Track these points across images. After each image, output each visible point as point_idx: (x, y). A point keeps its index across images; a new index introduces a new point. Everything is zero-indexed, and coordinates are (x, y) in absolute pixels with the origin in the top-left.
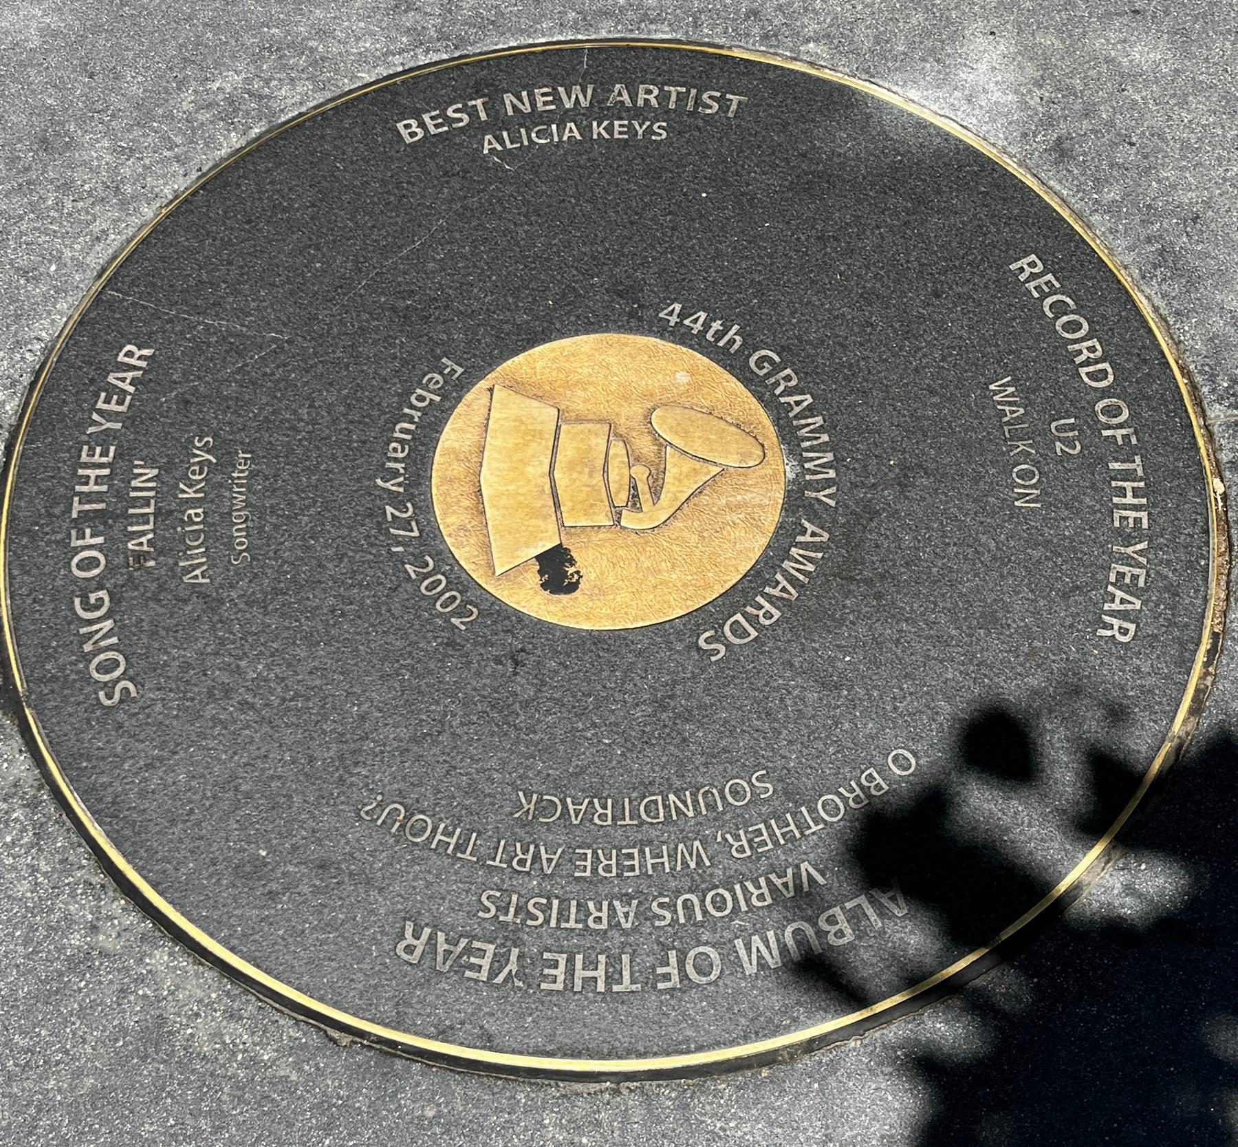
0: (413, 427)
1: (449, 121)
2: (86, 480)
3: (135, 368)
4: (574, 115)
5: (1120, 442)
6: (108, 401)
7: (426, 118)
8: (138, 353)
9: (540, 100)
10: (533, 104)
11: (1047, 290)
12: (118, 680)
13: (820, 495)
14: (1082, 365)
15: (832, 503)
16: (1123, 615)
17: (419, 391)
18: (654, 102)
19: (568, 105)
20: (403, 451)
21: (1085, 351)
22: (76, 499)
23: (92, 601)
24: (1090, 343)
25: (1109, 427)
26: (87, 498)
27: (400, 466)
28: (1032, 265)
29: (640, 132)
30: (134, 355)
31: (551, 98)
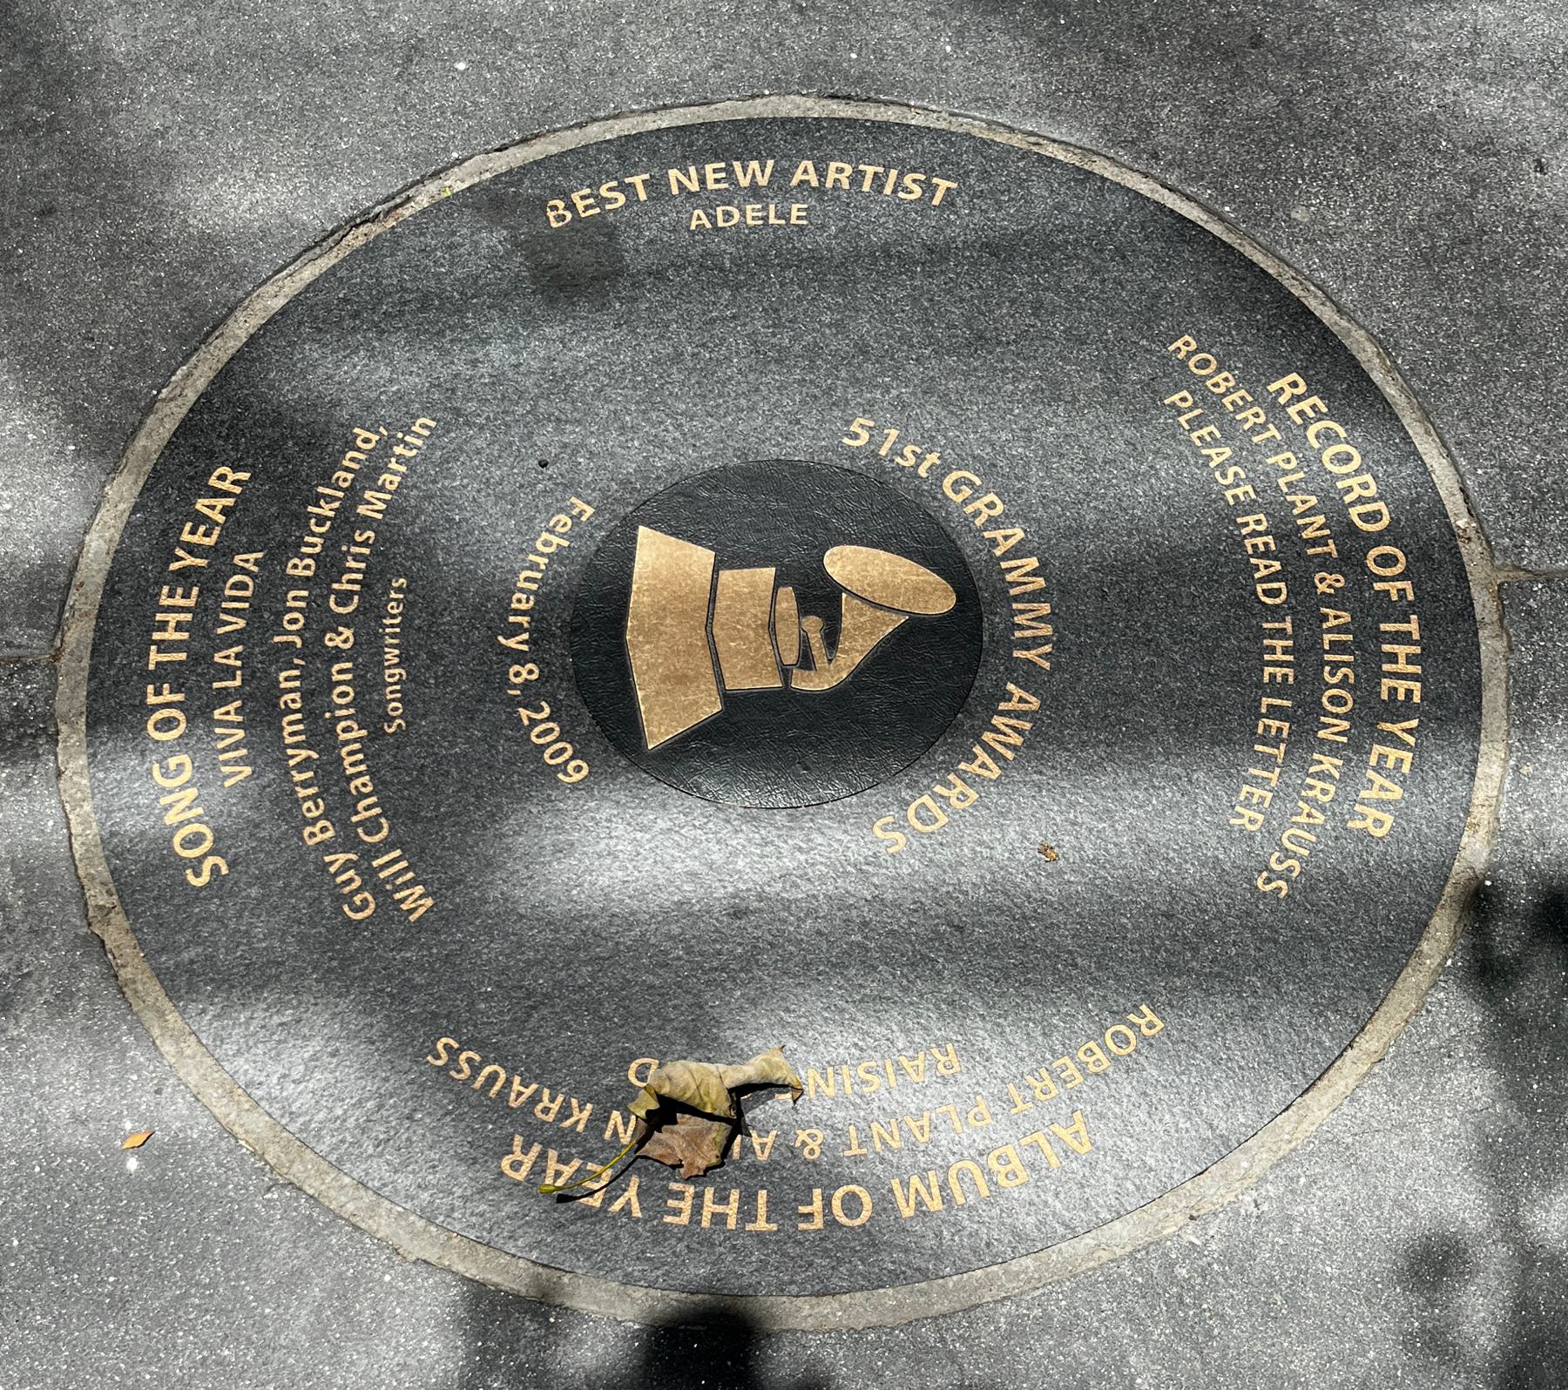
0: (539, 576)
1: (601, 201)
2: (720, 1219)
3: (226, 494)
4: (755, 192)
5: (1395, 598)
6: (193, 532)
7: (575, 197)
8: (231, 476)
9: (710, 177)
10: (702, 181)
11: (1312, 415)
12: (205, 856)
13: (1030, 655)
14: (1352, 504)
15: (1047, 665)
16: (1381, 804)
17: (545, 536)
18: (846, 185)
19: (744, 182)
20: (317, 807)
21: (1287, 388)
22: (153, 648)
23: (172, 767)
24: (1360, 479)
25: (1383, 579)
26: (164, 647)
27: (524, 620)
28: (1294, 385)
29: (632, 1193)
30: (227, 478)
31: (723, 175)
